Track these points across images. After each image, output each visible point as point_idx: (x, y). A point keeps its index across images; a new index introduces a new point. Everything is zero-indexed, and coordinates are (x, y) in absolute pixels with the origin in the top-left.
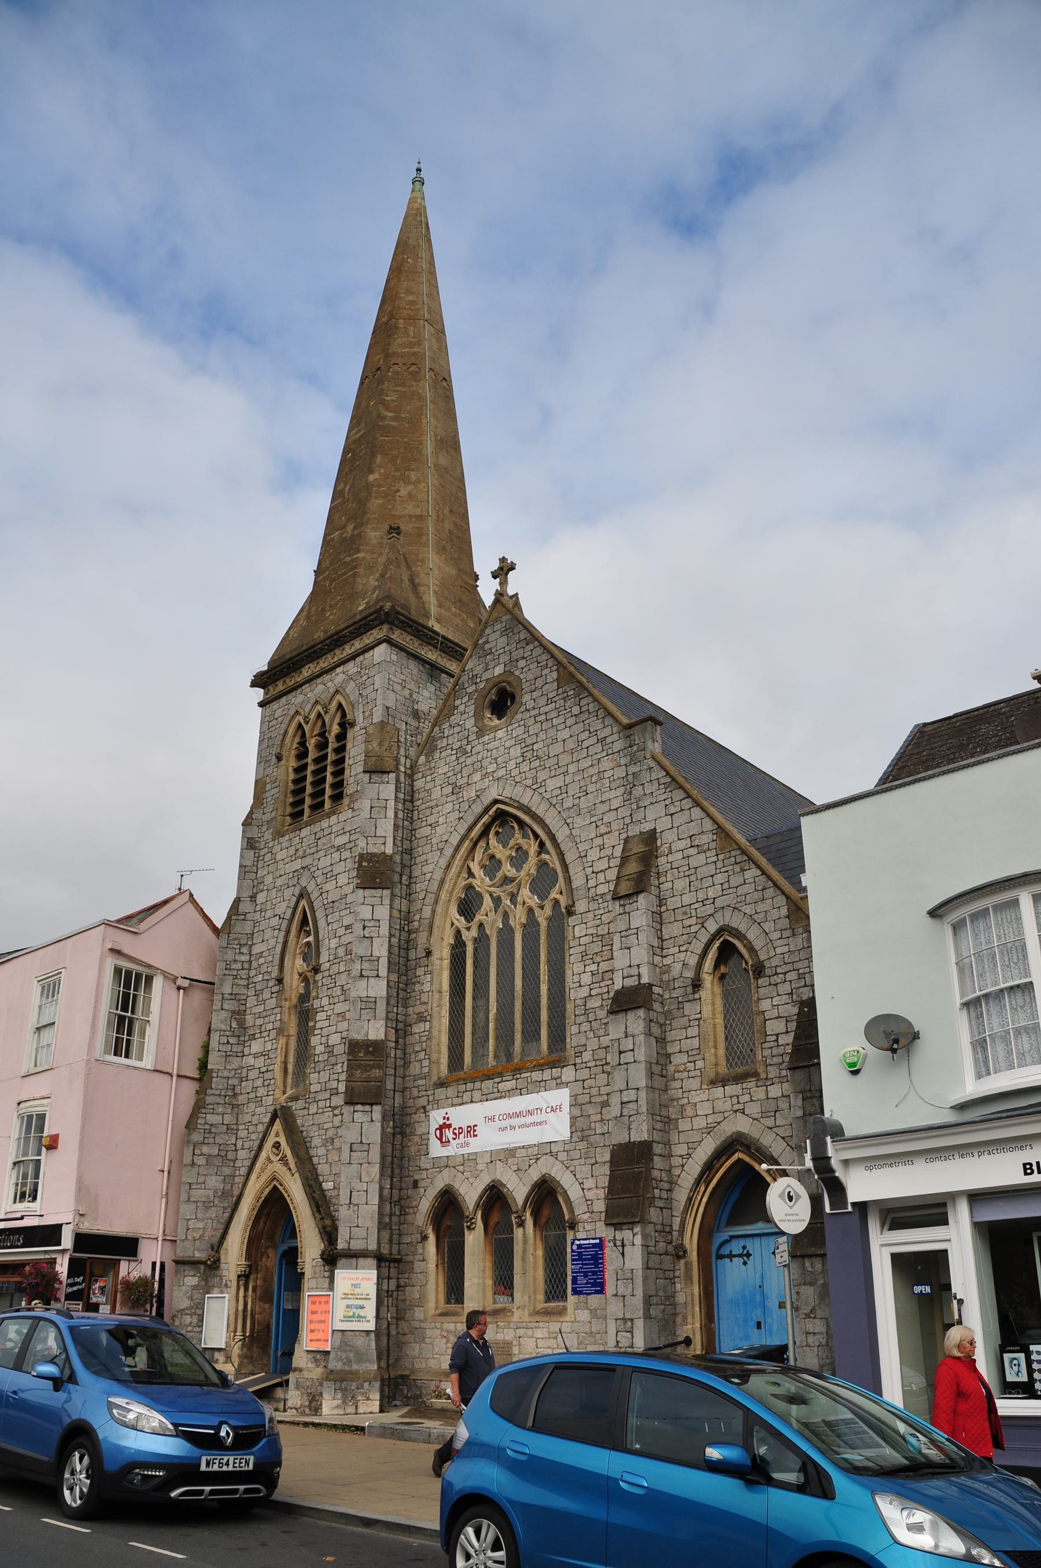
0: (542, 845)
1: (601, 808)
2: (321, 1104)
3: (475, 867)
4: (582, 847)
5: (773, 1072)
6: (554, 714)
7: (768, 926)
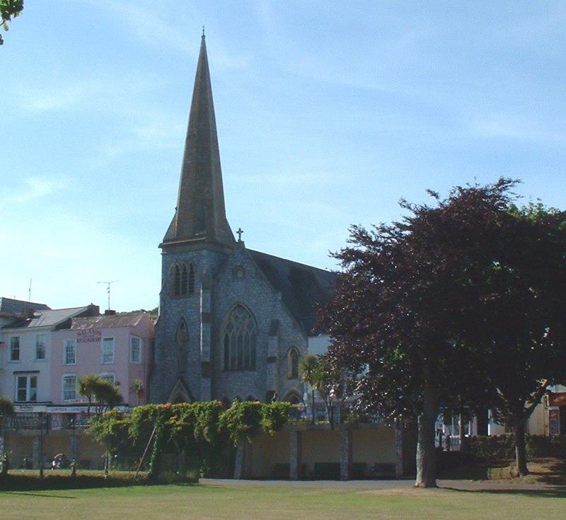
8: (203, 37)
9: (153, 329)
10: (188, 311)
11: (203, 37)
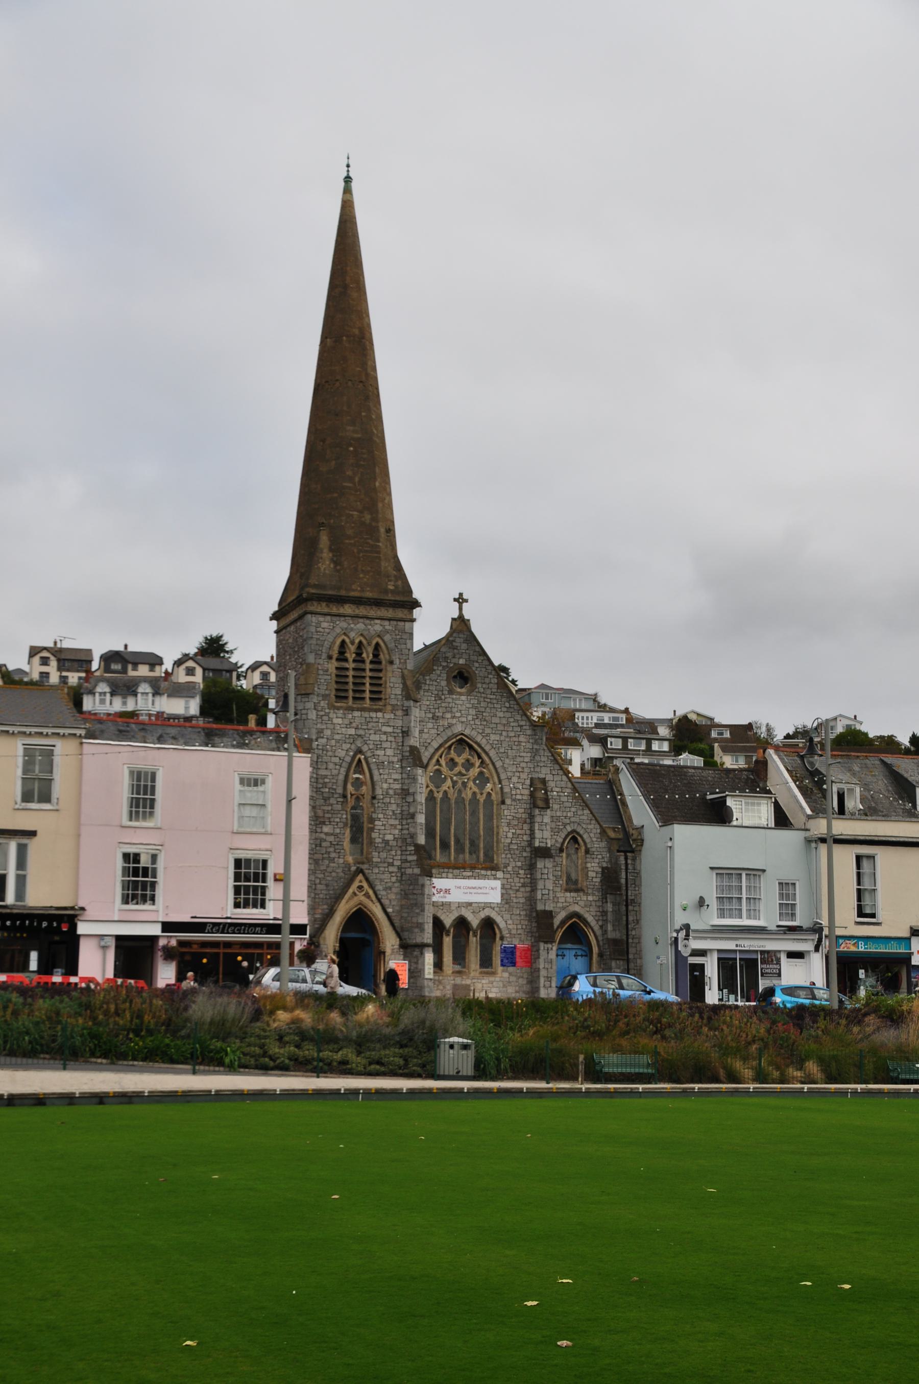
0: (483, 762)
1: (519, 759)
2: (382, 869)
3: (443, 762)
4: (509, 774)
5: (590, 891)
6: (495, 701)
7: (592, 835)
8: (348, 180)
9: (598, 1068)
10: (373, 737)
11: (348, 180)
